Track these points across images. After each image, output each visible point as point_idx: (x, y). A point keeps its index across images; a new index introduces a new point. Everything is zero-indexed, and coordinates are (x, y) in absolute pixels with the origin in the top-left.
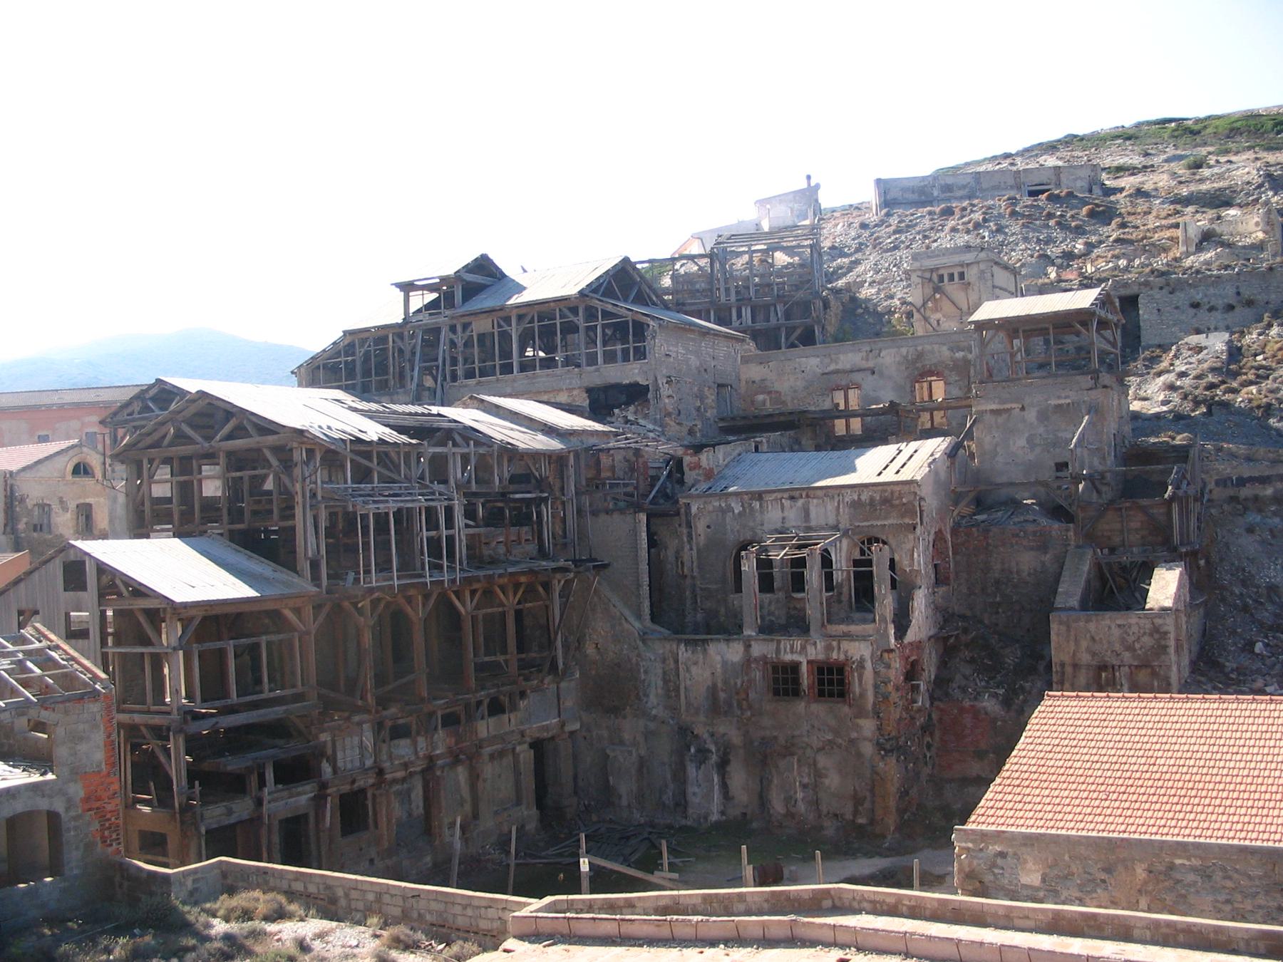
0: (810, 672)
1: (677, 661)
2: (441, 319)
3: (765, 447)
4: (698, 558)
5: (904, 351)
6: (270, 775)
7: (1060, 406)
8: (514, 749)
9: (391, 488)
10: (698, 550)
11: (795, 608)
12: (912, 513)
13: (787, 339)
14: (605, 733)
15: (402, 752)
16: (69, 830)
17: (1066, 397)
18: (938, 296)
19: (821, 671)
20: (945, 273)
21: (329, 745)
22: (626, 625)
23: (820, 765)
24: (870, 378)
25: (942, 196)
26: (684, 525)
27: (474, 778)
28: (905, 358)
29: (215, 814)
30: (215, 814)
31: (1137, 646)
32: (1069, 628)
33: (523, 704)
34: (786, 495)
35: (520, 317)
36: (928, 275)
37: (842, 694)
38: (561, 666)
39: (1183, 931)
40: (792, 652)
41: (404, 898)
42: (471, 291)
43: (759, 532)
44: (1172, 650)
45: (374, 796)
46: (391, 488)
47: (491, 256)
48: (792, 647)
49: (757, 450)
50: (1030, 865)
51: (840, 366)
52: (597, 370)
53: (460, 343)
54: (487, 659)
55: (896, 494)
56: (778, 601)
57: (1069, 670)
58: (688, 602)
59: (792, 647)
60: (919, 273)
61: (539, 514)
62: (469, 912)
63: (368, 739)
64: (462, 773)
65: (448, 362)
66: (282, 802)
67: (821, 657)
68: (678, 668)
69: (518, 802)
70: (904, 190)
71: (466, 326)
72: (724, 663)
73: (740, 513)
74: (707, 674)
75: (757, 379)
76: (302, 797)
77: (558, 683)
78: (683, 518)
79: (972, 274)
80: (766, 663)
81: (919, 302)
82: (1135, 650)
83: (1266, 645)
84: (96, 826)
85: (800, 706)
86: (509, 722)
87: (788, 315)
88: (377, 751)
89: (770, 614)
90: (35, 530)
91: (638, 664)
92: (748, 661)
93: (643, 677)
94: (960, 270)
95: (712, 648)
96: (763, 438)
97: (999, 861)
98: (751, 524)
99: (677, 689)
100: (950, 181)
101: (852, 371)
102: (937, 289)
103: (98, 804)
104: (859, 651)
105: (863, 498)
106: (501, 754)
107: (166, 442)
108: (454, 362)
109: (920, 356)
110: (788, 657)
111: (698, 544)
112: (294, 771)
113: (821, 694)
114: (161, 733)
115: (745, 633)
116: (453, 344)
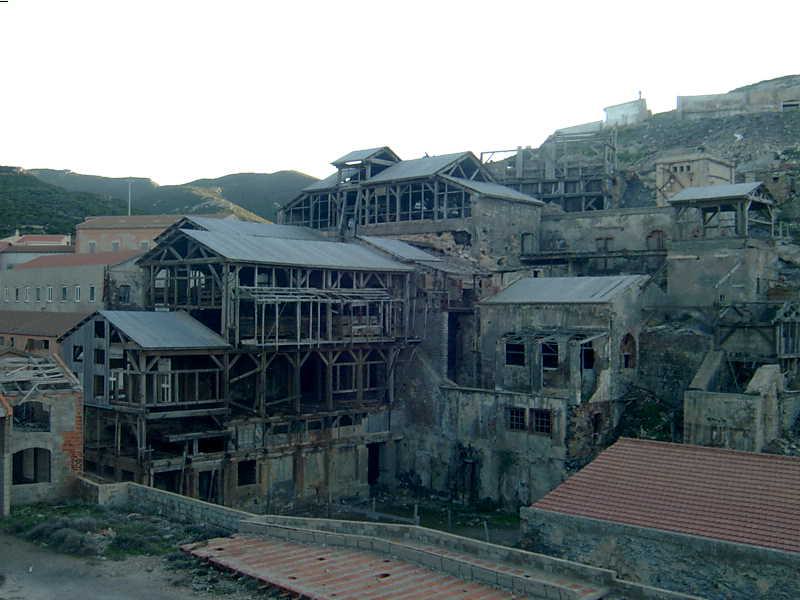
2: (358, 186)
6: (196, 447)
8: (356, 447)
13: (586, 203)
17: (725, 253)
20: (678, 166)
21: (234, 433)
27: (327, 461)
29: (160, 465)
30: (160, 465)
31: (736, 416)
36: (667, 167)
38: (392, 400)
41: (203, 509)
42: (377, 170)
44: (758, 421)
45: (260, 465)
47: (392, 148)
49: (536, 276)
51: (602, 225)
56: (525, 371)
57: (693, 427)
62: (229, 519)
63: (259, 434)
64: (319, 457)
65: (360, 213)
66: (203, 463)
70: (696, 103)
71: (372, 191)
72: (483, 407)
75: (553, 230)
77: (390, 410)
79: (694, 167)
80: (506, 408)
84: (69, 459)
85: (523, 436)
87: (587, 188)
92: (496, 405)
94: (688, 164)
96: (540, 269)
99: (456, 420)
104: (558, 405)
106: (347, 448)
107: (163, 257)
110: (520, 405)
112: (210, 446)
113: (512, 427)
114: (135, 416)
116: (364, 202)
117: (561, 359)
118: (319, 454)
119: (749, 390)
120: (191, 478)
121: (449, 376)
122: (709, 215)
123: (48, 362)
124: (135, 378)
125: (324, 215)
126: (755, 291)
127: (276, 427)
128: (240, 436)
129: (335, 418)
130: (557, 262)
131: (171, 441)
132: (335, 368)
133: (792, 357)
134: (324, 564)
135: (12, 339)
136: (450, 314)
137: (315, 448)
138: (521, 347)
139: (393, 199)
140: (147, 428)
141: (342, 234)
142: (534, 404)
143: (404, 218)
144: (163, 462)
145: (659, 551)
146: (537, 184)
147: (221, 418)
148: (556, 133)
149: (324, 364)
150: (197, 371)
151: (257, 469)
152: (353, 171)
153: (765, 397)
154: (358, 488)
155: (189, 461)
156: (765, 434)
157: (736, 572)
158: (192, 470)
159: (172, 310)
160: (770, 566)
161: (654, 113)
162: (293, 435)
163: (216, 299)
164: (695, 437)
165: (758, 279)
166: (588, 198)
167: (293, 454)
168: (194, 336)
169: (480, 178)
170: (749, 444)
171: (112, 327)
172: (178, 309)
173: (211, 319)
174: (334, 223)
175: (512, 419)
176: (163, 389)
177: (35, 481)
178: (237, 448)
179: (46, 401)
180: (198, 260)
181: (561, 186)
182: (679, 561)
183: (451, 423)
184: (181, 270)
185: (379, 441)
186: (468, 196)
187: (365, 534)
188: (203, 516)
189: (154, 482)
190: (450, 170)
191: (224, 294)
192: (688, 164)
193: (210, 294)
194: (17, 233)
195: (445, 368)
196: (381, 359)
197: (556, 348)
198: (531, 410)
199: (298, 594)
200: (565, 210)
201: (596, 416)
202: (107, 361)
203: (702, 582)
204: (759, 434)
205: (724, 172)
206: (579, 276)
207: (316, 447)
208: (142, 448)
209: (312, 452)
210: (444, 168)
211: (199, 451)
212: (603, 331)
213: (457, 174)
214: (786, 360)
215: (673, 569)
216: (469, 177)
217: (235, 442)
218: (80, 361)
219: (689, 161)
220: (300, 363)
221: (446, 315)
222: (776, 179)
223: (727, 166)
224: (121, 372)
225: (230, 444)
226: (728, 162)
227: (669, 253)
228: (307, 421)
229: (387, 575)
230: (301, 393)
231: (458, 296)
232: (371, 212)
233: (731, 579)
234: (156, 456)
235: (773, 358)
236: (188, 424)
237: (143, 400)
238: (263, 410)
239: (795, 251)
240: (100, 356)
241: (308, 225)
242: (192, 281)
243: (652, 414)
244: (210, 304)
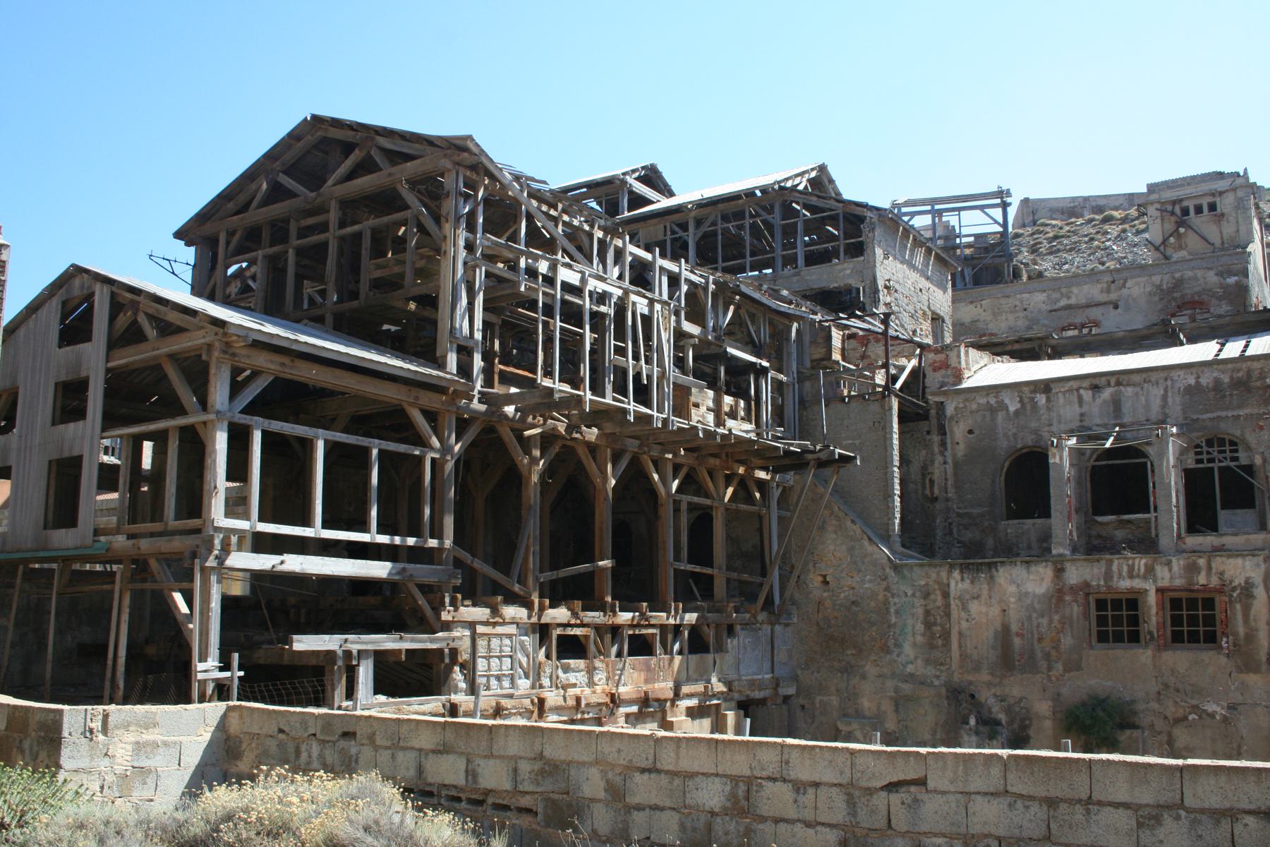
0: (1161, 605)
1: (946, 595)
4: (955, 474)
10: (956, 464)
11: (1099, 536)
14: (834, 700)
18: (1182, 230)
19: (1176, 604)
24: (1112, 312)
26: (935, 430)
28: (1159, 287)
33: (731, 643)
34: (1086, 384)
35: (699, 223)
36: (1170, 208)
37: (1211, 638)
38: (777, 600)
40: (1131, 576)
43: (1046, 435)
47: (660, 168)
48: (1131, 569)
51: (1073, 301)
52: (797, 274)
55: (1256, 374)
59: (1131, 569)
60: (1158, 206)
67: (1178, 582)
68: (948, 606)
72: (1022, 596)
73: (1017, 412)
74: (995, 611)
78: (934, 422)
80: (1087, 595)
85: (1143, 656)
91: (886, 602)
92: (1059, 594)
93: (893, 620)
94: (1210, 199)
98: (1034, 425)
99: (946, 635)
100: (1101, 203)
101: (1088, 306)
102: (1180, 224)
105: (1203, 381)
109: (1178, 284)
110: (1125, 584)
111: (954, 456)
113: (1177, 638)
115: (1054, 552)
128: (481, 651)
132: (677, 503)
142: (1170, 574)
183: (932, 646)
217: (469, 669)
225: (458, 675)
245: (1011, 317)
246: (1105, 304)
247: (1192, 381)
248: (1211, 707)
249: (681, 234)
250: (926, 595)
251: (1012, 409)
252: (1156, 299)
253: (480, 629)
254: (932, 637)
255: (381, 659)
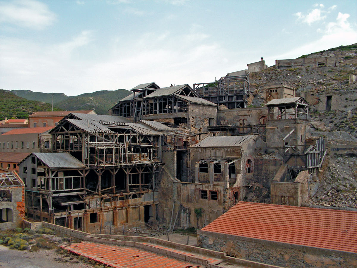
0: (209, 193)
1: (180, 188)
2: (142, 99)
3: (216, 135)
4: (191, 163)
5: (257, 111)
7: (286, 128)
8: (139, 207)
9: (107, 143)
10: (191, 161)
12: (240, 155)
13: (237, 105)
15: (107, 205)
16: (14, 213)
17: (288, 126)
18: (270, 96)
20: (272, 90)
21: (88, 202)
22: (170, 179)
23: (211, 216)
25: (294, 65)
27: (127, 213)
28: (258, 112)
30: (58, 215)
31: (291, 192)
32: (275, 186)
34: (211, 148)
36: (268, 90)
37: (216, 199)
39: (208, 252)
41: (71, 232)
45: (99, 215)
46: (107, 143)
50: (211, 240)
51: (242, 114)
52: (176, 114)
53: (145, 105)
54: (132, 185)
57: (274, 196)
58: (189, 174)
61: (150, 151)
62: (80, 236)
64: (124, 211)
67: (212, 190)
68: (180, 190)
69: (140, 220)
70: (284, 63)
71: (147, 101)
74: (187, 192)
76: (80, 213)
77: (153, 192)
81: (265, 98)
82: (290, 193)
83: (331, 193)
84: (20, 213)
86: (140, 200)
87: (237, 99)
88: (100, 204)
89: (207, 178)
90: (45, 147)
92: (196, 189)
94: (276, 89)
95: (188, 185)
96: (216, 133)
97: (205, 238)
98: (203, 155)
99: (180, 195)
100: (296, 61)
101: (244, 115)
103: (20, 208)
104: (220, 189)
106: (135, 208)
107: (59, 130)
108: (144, 110)
110: (205, 189)
113: (212, 199)
116: (144, 106)
117: (222, 170)
118: (123, 210)
119: (296, 181)
120: (71, 220)
121: (177, 178)
122: (283, 110)
123: (11, 174)
124: (48, 180)
125: (128, 111)
126: (300, 141)
127: (105, 199)
128: (90, 203)
129: (130, 195)
130: (222, 130)
131: (62, 205)
133: (314, 167)
134: (115, 252)
135: (1, 164)
136: (177, 152)
137: (122, 208)
138: (206, 166)
139: (156, 104)
140: (52, 200)
141: (135, 119)
142: (211, 188)
143: (160, 112)
144: (59, 214)
145: (249, 246)
146: (217, 97)
147: (82, 195)
148: (227, 75)
149: (111, 174)
150: (72, 177)
151: (98, 216)
152: (140, 93)
153: (302, 183)
154: (140, 224)
155: (70, 213)
156: (302, 198)
157: (276, 252)
158: (71, 217)
159: (63, 152)
160: (289, 250)
161: (269, 66)
162: (112, 202)
163: (80, 148)
164: (275, 200)
165: (301, 136)
166: (238, 103)
167: (113, 210)
168: (73, 163)
169: (191, 95)
170: (295, 202)
171: (38, 159)
172: (65, 152)
173: (78, 156)
174: (132, 114)
175: (202, 195)
176: (61, 184)
177: (7, 221)
178: (89, 208)
179: (10, 190)
180: (73, 132)
181: (227, 98)
182: (256, 249)
184: (67, 135)
185: (149, 204)
186: (185, 103)
187: (133, 241)
188: (71, 235)
189: (56, 222)
190: (179, 93)
191: (83, 145)
192: (276, 89)
193: (78, 145)
194: (6, 118)
195: (175, 174)
196: (150, 171)
197: (220, 166)
198: (210, 191)
199: (102, 263)
200: (229, 108)
201: (236, 193)
202: (36, 173)
203: (264, 257)
204: (300, 199)
205: (292, 92)
206: (232, 135)
207: (122, 207)
208: (51, 208)
209: (121, 209)
210: (176, 92)
211: (74, 209)
212: (238, 158)
213: (182, 94)
214: (311, 168)
215: (254, 252)
216: (187, 95)
217: (89, 205)
218: (27, 173)
219: (276, 88)
220: (115, 173)
221: (176, 152)
222: (312, 94)
223: (292, 90)
224: (43, 177)
226: (292, 88)
227: (267, 126)
228: (118, 197)
229: (138, 256)
230: (116, 185)
231: (181, 145)
232: (147, 110)
233: (275, 255)
234: (56, 211)
235: (306, 168)
236: (70, 198)
237: (51, 189)
238: (100, 193)
239: (319, 124)
240: (34, 171)
241: (122, 115)
242: (71, 140)
243: (260, 191)
244: (78, 150)
245: (230, 117)
246: (248, 115)
247: (227, 150)
248: (215, 211)
249: (156, 102)
250: (178, 188)
251: (200, 152)
252: (257, 115)
253: (90, 199)
254: (178, 195)
255: (75, 205)
